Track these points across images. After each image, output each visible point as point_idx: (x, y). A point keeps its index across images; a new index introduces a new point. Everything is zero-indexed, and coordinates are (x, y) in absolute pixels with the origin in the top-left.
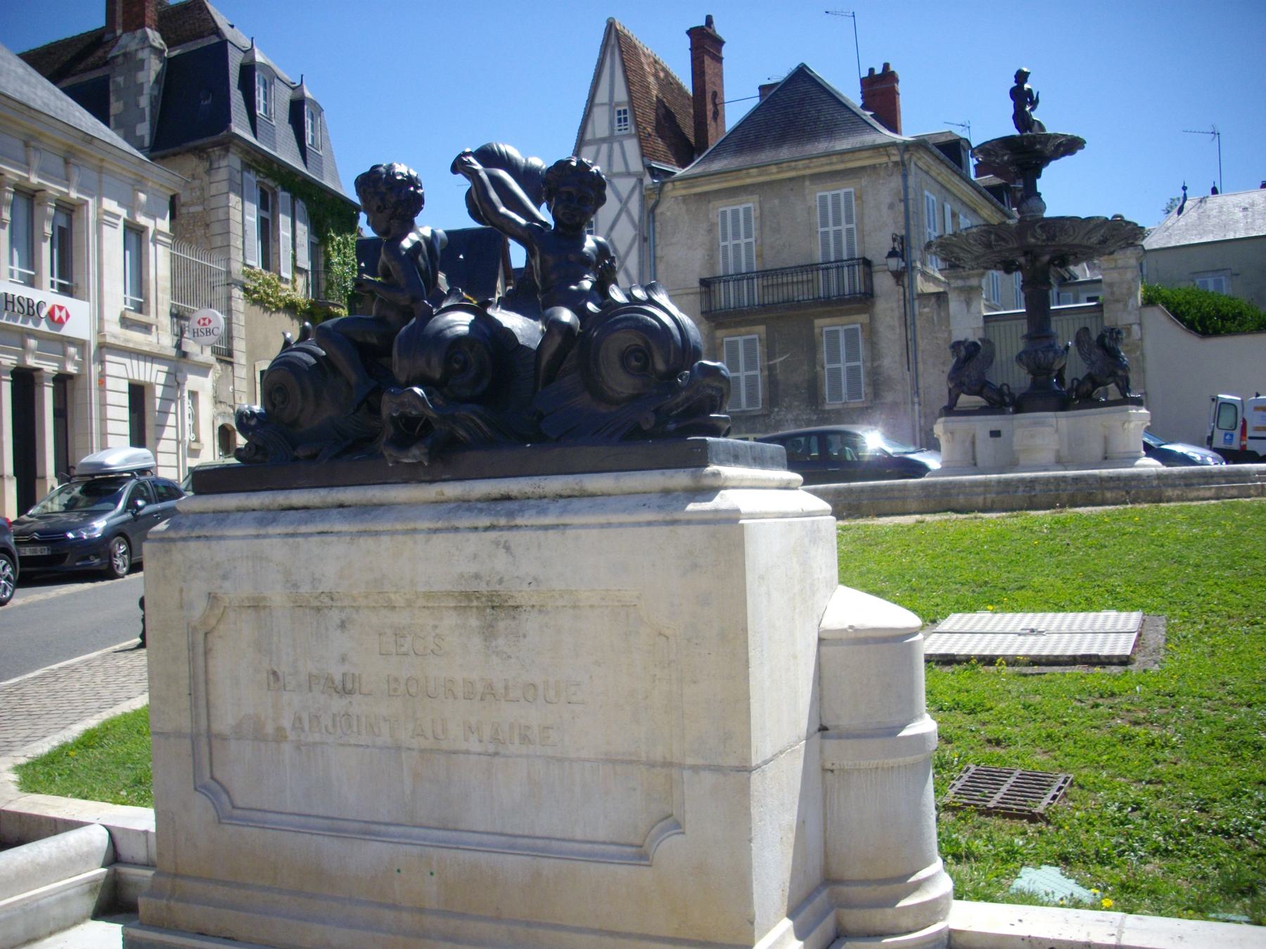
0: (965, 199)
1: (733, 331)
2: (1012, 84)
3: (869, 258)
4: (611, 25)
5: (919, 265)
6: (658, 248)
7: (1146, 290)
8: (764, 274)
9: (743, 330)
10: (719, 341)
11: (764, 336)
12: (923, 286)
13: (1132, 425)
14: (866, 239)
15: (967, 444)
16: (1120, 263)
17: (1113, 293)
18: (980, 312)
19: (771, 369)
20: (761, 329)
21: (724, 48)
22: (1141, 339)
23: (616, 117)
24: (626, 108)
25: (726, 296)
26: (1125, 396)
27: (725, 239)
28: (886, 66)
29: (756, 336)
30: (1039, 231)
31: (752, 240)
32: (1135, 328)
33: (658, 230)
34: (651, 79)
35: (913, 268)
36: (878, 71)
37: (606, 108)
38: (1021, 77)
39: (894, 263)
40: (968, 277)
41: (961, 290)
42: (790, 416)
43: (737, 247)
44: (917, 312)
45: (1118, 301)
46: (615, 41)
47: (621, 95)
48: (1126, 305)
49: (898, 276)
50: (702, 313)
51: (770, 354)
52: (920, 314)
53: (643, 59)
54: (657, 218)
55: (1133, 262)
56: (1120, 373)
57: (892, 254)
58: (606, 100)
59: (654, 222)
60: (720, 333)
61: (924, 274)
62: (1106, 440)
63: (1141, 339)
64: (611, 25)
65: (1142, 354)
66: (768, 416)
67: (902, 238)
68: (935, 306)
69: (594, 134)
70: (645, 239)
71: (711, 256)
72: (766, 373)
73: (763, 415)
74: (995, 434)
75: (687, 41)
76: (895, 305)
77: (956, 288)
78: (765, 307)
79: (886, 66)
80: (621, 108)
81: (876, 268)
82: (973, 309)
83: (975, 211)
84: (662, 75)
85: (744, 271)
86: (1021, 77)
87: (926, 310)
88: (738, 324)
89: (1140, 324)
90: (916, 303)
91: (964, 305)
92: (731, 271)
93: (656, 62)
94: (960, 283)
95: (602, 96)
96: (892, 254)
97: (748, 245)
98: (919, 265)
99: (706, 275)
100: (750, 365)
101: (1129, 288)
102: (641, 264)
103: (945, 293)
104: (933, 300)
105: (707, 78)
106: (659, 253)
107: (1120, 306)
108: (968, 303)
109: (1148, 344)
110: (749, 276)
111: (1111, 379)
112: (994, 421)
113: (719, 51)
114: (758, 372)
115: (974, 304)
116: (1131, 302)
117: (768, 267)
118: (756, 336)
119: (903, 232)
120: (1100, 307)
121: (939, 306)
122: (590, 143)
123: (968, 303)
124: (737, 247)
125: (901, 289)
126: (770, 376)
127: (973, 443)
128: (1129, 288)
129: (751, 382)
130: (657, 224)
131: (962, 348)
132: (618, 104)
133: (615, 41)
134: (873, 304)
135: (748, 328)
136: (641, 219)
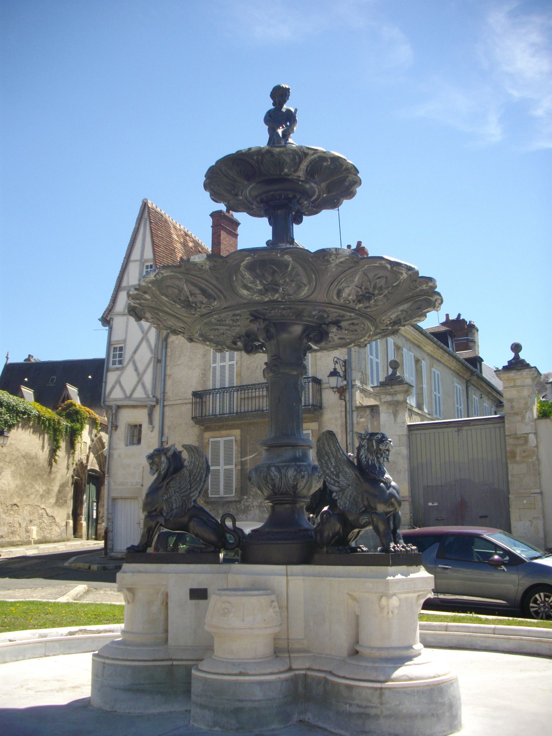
0: (408, 336)
1: (217, 433)
2: (269, 105)
3: (319, 377)
4: (145, 205)
5: (358, 383)
6: (168, 368)
7: (542, 404)
8: (242, 388)
9: (224, 432)
10: (206, 441)
11: (239, 438)
12: (359, 399)
13: (394, 601)
14: (318, 362)
15: (156, 607)
16: (518, 383)
17: (512, 407)
18: (404, 422)
19: (243, 464)
20: (237, 432)
21: (239, 228)
22: (537, 446)
23: (145, 270)
24: (152, 263)
25: (215, 406)
26: (386, 549)
27: (215, 362)
28: (359, 243)
29: (233, 438)
30: (247, 275)
31: (234, 362)
32: (532, 437)
33: (169, 354)
34: (178, 246)
35: (353, 386)
36: (354, 246)
37: (138, 264)
38: (280, 95)
39: (334, 381)
40: (395, 393)
41: (389, 403)
42: (255, 503)
43: (223, 367)
44: (355, 422)
45: (516, 414)
46: (147, 215)
47: (149, 254)
48: (523, 417)
49: (342, 391)
50: (193, 418)
51: (243, 453)
52: (358, 423)
53: (172, 231)
54: (169, 346)
55: (529, 381)
56: (381, 508)
57: (334, 373)
58: (138, 258)
59: (166, 348)
60: (207, 435)
61: (363, 391)
62: (356, 623)
63: (537, 446)
64: (145, 205)
65: (538, 459)
66: (239, 502)
67: (345, 362)
68: (369, 417)
69: (128, 282)
70: (159, 361)
71: (204, 375)
72: (239, 467)
73: (236, 502)
74: (199, 594)
75: (210, 221)
76: (338, 416)
77: (386, 402)
78: (240, 415)
79: (359, 243)
80: (149, 264)
81: (324, 386)
82: (399, 420)
83: (419, 347)
84: (191, 244)
85: (227, 386)
86: (280, 95)
87: (363, 420)
88: (220, 428)
89: (536, 434)
90: (355, 414)
91: (392, 417)
92: (218, 386)
93: (186, 235)
94: (389, 398)
95: (136, 255)
96: (334, 373)
97: (231, 366)
98: (358, 383)
99: (199, 389)
100: (228, 461)
101: (526, 404)
102: (155, 379)
103: (377, 406)
104: (368, 411)
105: (222, 247)
106: (168, 372)
107: (519, 418)
108: (395, 414)
109: (543, 452)
110: (231, 389)
111: (364, 519)
112: (198, 574)
113: (236, 229)
114: (233, 467)
115: (400, 415)
116: (528, 415)
117: (245, 384)
118: (233, 438)
119: (346, 357)
120: (502, 418)
121: (373, 417)
122: (125, 288)
123: (395, 414)
124: (223, 367)
125: (344, 403)
126: (242, 470)
127: (166, 605)
128: (526, 404)
129: (228, 473)
130: (169, 350)
131: (163, 458)
132: (146, 261)
133: (147, 215)
134: (321, 415)
135: (228, 432)
136: (156, 346)
